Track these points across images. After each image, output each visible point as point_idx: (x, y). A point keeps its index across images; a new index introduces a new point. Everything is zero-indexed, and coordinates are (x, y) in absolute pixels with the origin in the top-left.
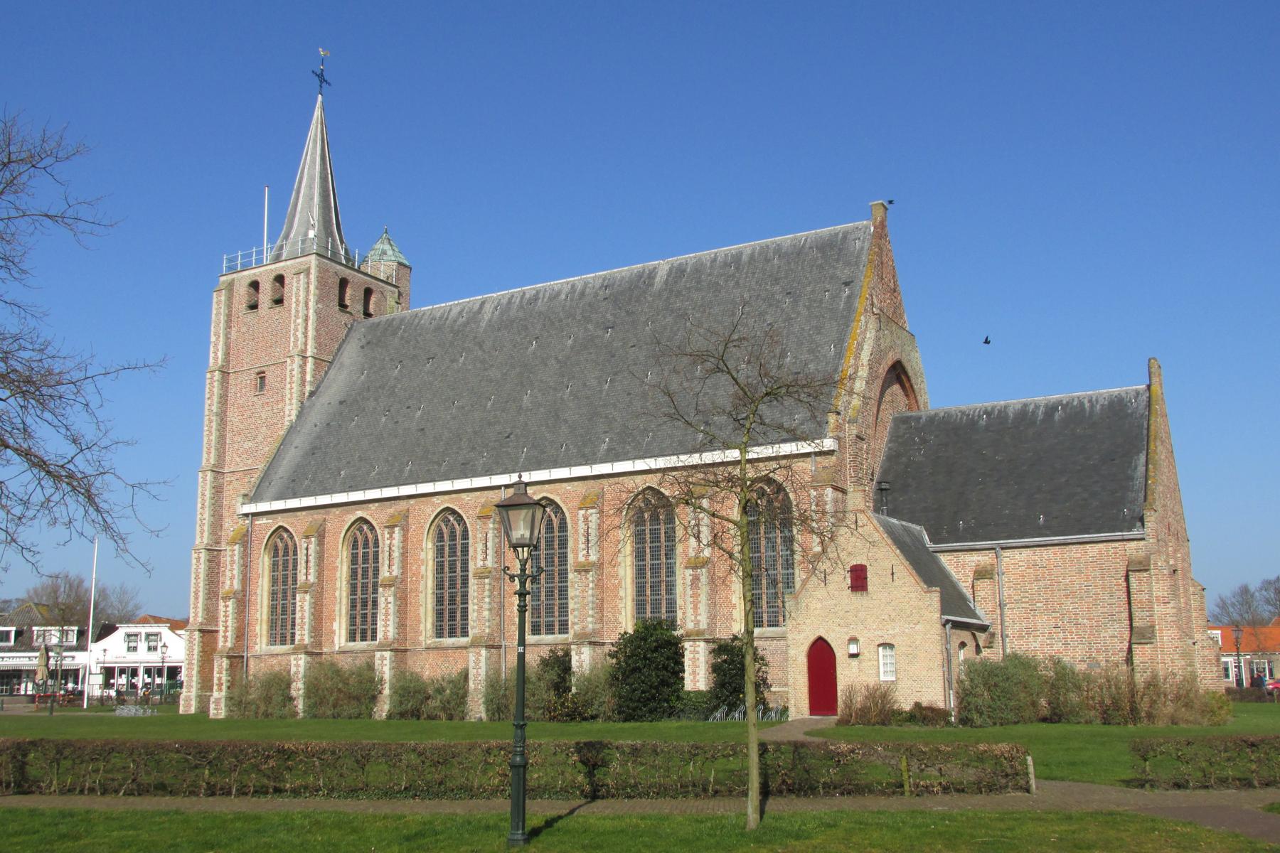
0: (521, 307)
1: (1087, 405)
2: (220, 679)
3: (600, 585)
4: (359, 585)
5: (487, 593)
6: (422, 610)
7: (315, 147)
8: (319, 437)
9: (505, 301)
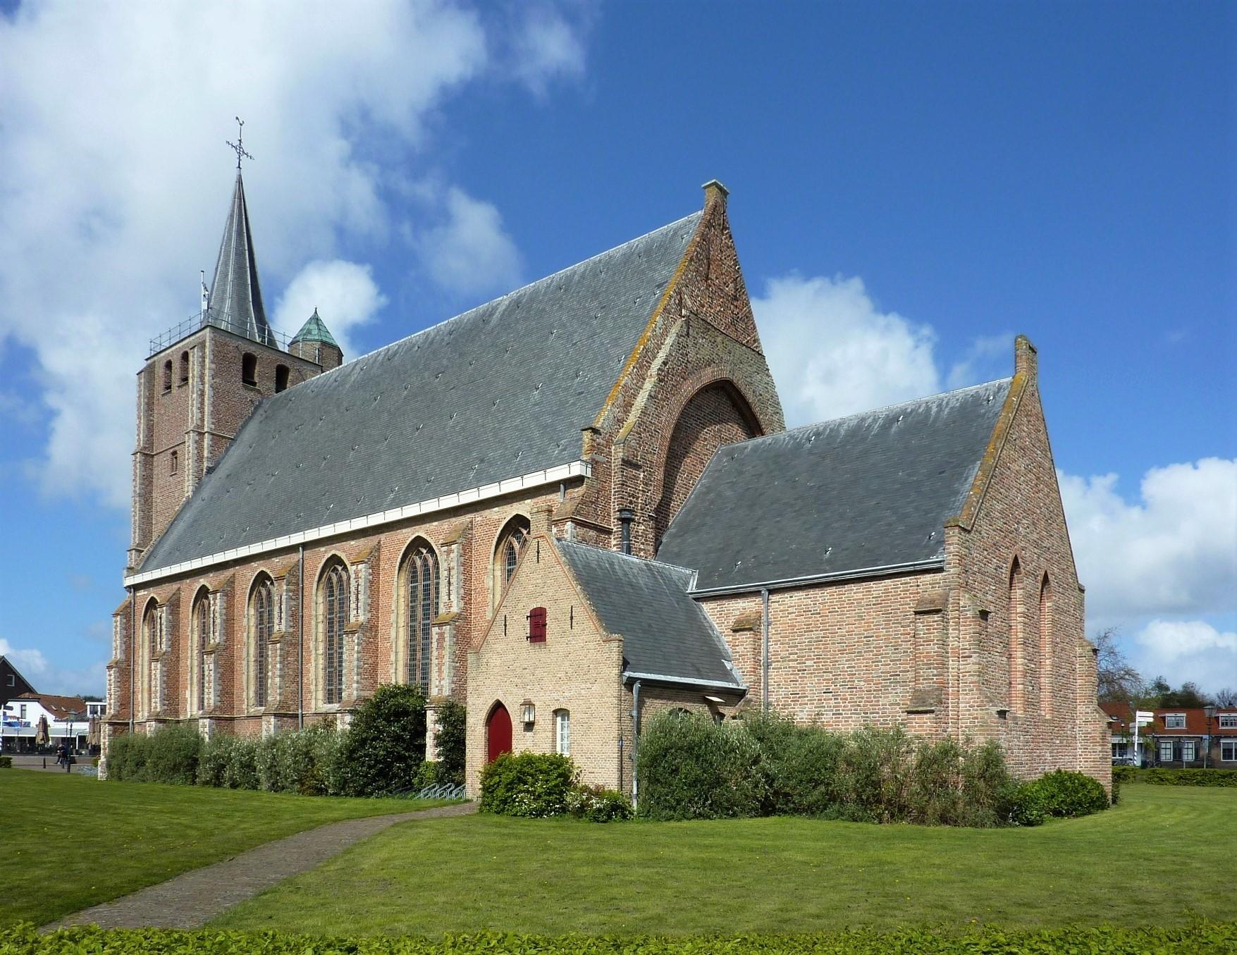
1: (934, 409)
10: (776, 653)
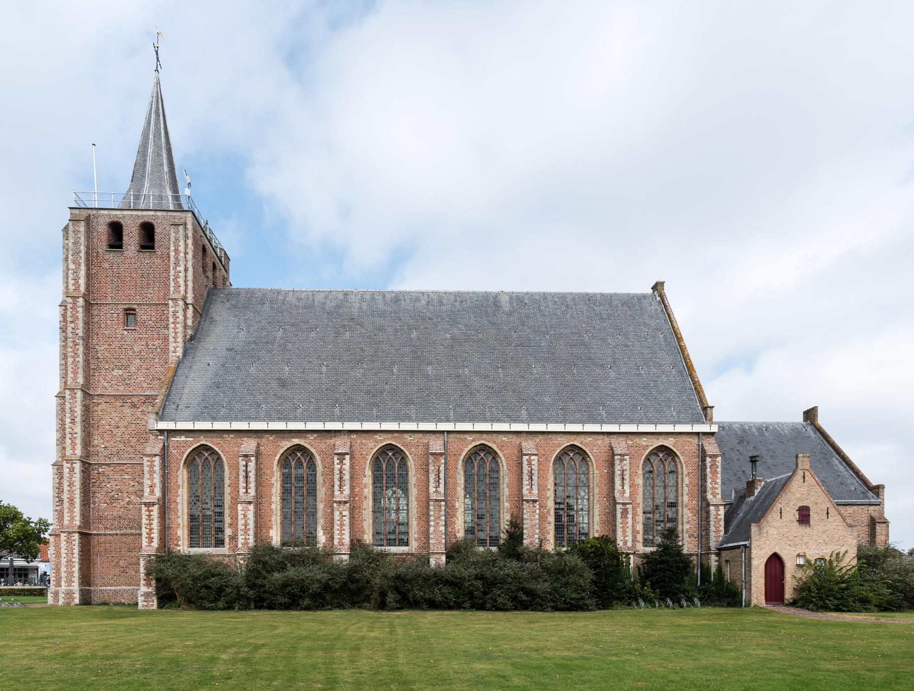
5: (443, 513)
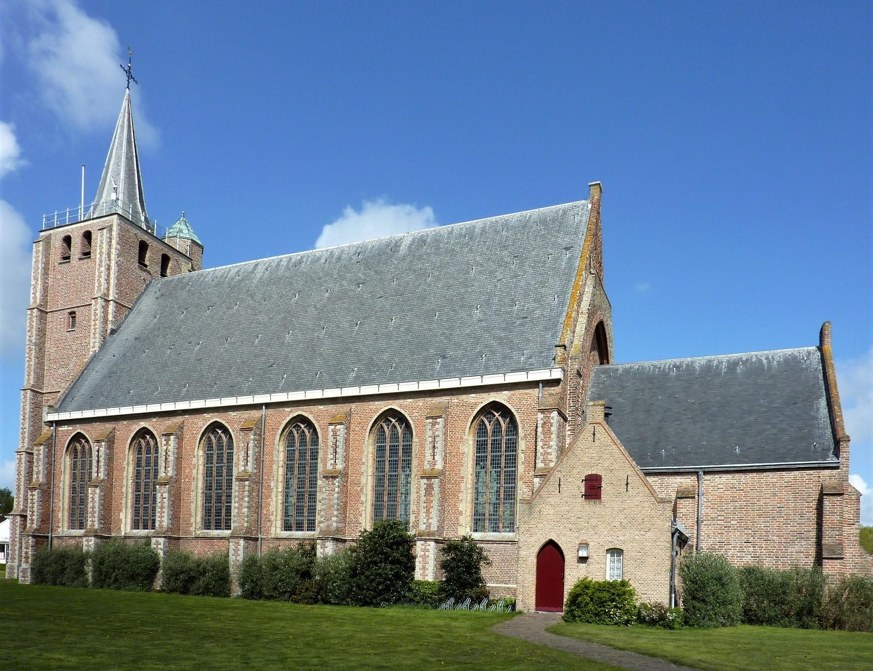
0: (288, 268)
2: (27, 553)
3: (344, 490)
4: (143, 484)
5: (246, 493)
6: (193, 506)
7: (122, 132)
8: (116, 365)
9: (274, 264)
10: (707, 515)
